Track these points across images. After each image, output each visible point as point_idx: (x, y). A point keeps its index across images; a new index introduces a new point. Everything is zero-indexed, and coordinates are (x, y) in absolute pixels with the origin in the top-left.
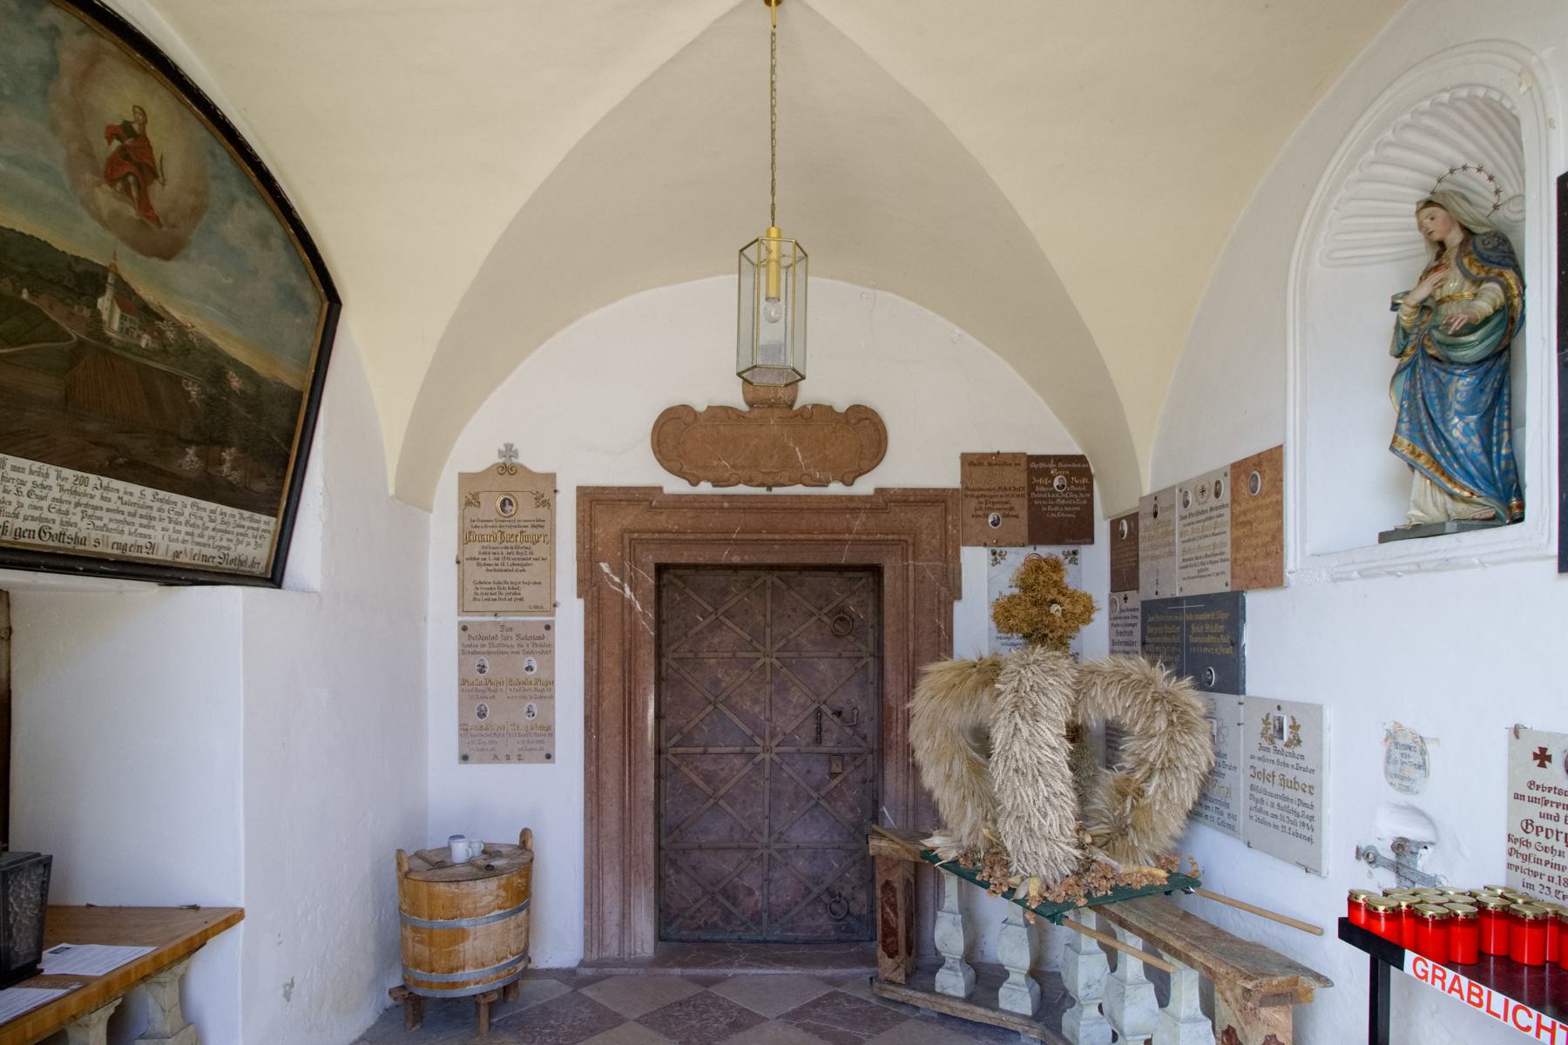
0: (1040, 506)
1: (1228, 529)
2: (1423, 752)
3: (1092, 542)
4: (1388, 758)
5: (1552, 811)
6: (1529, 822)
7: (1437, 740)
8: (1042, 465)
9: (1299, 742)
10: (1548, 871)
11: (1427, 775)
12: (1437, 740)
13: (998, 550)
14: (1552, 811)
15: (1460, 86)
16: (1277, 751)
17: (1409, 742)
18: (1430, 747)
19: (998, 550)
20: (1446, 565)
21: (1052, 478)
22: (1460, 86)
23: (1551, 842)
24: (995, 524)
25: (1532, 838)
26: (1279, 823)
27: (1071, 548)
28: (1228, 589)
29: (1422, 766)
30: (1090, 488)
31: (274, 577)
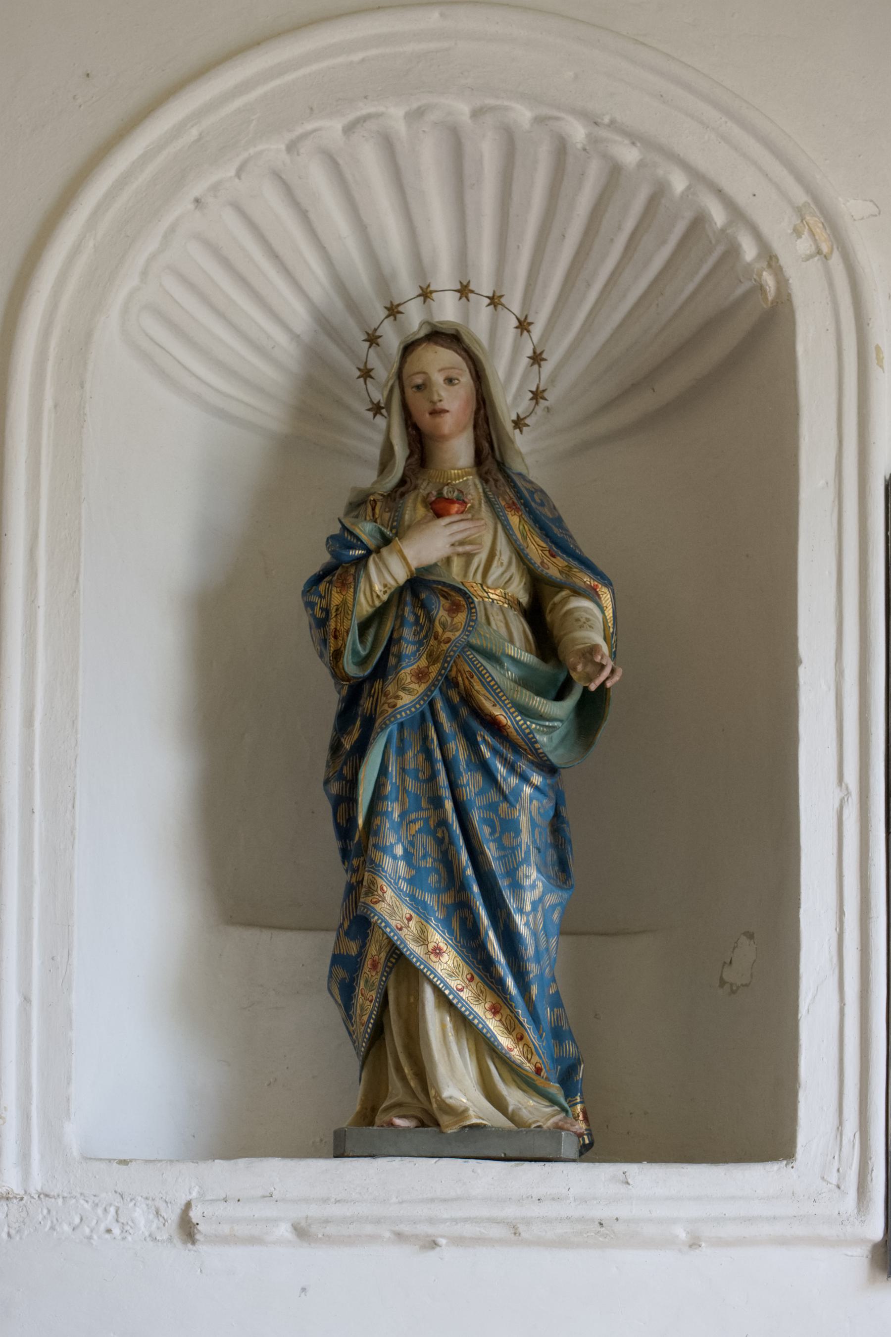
15: (634, 138)
20: (602, 1232)
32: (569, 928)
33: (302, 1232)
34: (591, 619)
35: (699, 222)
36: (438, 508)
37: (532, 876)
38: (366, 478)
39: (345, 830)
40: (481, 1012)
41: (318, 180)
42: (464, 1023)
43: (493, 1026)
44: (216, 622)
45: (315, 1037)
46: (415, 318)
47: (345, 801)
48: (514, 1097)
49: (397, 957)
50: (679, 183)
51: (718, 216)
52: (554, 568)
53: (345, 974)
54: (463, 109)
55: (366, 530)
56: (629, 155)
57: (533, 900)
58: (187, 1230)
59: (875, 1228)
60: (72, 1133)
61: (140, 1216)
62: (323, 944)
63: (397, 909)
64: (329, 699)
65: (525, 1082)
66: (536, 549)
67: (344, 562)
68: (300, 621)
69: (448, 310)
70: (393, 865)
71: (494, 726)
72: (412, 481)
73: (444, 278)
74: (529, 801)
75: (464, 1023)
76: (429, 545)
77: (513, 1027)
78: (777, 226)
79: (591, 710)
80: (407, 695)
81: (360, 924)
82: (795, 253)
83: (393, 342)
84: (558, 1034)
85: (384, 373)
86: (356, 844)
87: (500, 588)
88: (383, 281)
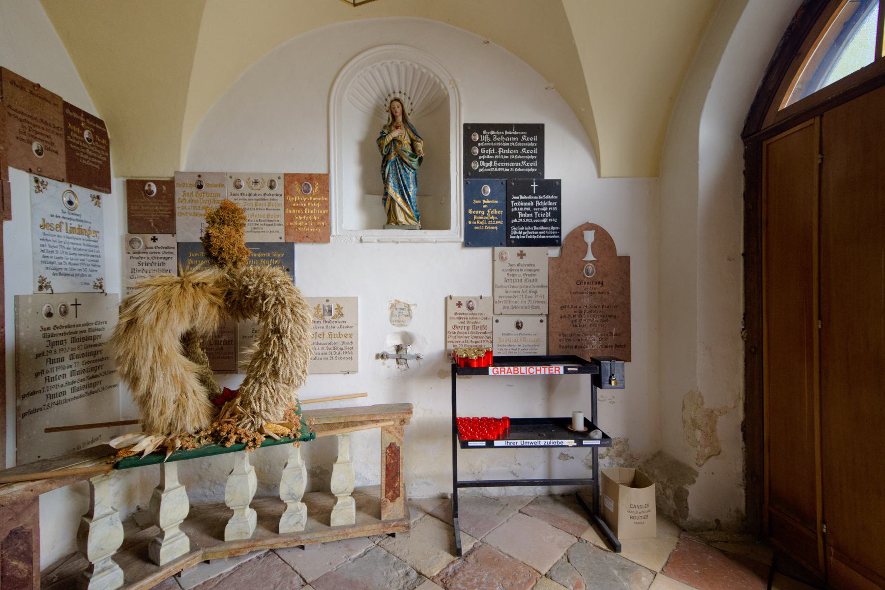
0: (74, 150)
1: (282, 208)
2: (409, 310)
3: (110, 192)
4: (392, 315)
5: (462, 320)
6: (455, 326)
7: (416, 305)
8: (75, 115)
9: (342, 315)
10: (462, 339)
11: (411, 318)
12: (416, 305)
13: (40, 179)
14: (462, 320)
15: (425, 67)
16: (326, 322)
17: (402, 306)
18: (412, 308)
19: (40, 179)
20: (423, 241)
21: (83, 130)
22: (425, 67)
23: (463, 330)
24: (39, 152)
25: (456, 331)
26: (322, 356)
27: (96, 193)
28: (283, 241)
29: (409, 315)
30: (107, 150)
31: (624, 388)
32: (418, 194)
33: (379, 241)
34: (420, 146)
35: (435, 82)
36: (397, 128)
37: (412, 186)
38: (386, 122)
39: (384, 179)
40: (404, 207)
41: (377, 74)
42: (402, 209)
43: (406, 209)
44: (363, 146)
45: (381, 212)
46: (393, 97)
47: (384, 174)
48: (410, 220)
49: (392, 198)
50: (432, 76)
51: (438, 81)
52: (414, 138)
53: (385, 200)
54: (399, 62)
55: (386, 131)
56: (424, 71)
57: (412, 190)
58: (361, 241)
59: (462, 240)
60: (343, 226)
61: (354, 239)
62: (381, 197)
63: (393, 191)
64: (381, 158)
65: (412, 219)
66: (412, 135)
67: (382, 137)
68: (376, 145)
69: (398, 96)
70: (391, 185)
71: (406, 163)
72: (393, 124)
73: (397, 90)
74: (411, 175)
75: (402, 209)
76: (395, 134)
77: (409, 209)
78: (447, 83)
79: (420, 160)
80: (393, 157)
81: (386, 194)
82: (449, 87)
83: (389, 100)
84: (416, 211)
85: (388, 105)
86: (386, 181)
87: (406, 141)
88: (388, 90)
